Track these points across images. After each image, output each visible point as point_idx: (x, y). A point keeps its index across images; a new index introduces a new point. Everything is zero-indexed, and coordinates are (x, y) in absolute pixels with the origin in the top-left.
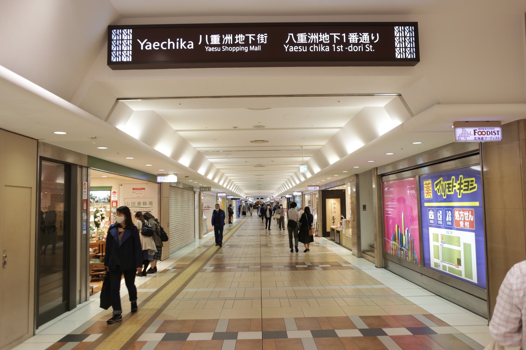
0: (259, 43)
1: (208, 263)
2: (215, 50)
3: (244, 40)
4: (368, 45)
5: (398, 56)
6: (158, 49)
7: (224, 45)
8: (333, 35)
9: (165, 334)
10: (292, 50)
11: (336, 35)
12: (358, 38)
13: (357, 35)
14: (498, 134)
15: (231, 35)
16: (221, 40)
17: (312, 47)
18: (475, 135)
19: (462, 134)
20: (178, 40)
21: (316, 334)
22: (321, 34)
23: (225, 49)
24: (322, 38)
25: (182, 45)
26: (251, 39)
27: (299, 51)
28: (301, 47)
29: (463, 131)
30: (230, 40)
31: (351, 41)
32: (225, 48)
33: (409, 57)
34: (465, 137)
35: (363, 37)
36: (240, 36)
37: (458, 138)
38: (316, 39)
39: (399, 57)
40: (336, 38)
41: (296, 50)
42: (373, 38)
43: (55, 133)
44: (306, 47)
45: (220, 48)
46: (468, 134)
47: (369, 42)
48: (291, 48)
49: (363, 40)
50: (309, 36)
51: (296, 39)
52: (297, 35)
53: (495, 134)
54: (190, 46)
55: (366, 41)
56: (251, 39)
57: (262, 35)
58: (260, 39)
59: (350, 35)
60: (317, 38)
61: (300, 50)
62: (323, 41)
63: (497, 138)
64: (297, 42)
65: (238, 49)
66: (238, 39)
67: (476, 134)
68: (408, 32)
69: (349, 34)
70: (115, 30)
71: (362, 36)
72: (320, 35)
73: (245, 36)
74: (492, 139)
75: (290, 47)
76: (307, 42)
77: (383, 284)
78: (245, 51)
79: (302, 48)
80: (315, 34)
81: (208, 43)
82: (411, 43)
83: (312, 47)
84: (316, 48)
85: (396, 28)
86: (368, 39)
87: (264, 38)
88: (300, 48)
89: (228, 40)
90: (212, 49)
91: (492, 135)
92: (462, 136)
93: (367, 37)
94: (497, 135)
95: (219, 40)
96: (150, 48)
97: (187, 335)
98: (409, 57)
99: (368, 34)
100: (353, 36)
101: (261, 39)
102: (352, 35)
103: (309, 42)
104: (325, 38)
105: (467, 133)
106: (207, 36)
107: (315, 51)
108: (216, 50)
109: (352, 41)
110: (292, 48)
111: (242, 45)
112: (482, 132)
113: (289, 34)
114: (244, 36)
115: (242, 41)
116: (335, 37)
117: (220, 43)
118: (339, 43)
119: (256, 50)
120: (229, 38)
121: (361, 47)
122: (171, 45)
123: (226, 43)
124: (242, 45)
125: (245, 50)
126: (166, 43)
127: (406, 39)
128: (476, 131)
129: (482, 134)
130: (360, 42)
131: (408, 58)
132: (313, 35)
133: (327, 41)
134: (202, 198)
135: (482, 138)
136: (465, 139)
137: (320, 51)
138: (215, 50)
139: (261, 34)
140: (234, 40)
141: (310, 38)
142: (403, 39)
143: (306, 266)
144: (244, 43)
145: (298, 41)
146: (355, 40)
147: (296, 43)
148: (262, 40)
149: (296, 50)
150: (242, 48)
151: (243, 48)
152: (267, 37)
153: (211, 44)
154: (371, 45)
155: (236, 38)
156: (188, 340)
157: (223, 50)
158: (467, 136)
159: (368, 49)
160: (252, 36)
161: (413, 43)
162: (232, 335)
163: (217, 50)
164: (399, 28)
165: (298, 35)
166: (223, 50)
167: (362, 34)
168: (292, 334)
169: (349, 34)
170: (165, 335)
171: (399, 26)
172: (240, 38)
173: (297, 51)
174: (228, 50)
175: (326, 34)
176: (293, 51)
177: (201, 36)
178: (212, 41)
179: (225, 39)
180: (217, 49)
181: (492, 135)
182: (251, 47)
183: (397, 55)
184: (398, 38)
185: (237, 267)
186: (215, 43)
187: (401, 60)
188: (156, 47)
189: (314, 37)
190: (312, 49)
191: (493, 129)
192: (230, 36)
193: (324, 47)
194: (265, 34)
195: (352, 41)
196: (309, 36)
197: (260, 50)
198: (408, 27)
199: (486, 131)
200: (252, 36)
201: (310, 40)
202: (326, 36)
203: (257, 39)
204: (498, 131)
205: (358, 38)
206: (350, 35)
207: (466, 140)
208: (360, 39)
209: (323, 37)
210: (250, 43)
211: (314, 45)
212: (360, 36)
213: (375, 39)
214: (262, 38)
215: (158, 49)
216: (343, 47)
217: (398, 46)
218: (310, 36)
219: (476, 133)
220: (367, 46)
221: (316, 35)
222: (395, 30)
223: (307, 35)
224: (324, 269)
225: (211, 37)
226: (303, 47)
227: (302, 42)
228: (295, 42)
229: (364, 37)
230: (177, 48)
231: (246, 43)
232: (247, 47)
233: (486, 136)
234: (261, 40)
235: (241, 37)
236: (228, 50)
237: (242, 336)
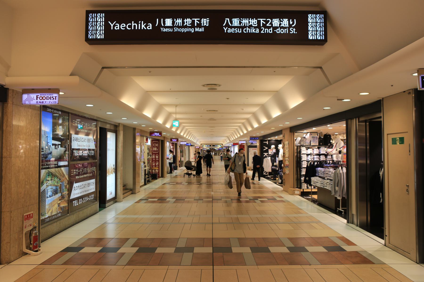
0: (202, 25)
1: (263, 196)
2: (168, 30)
4: (292, 28)
5: (310, 37)
6: (124, 29)
7: (176, 27)
8: (260, 20)
9: (138, 248)
10: (230, 32)
11: (263, 20)
12: (280, 23)
13: (279, 20)
14: (56, 99)
15: (181, 19)
16: (173, 23)
17: (246, 29)
18: (37, 99)
19: (27, 99)
20: (140, 22)
21: (254, 250)
22: (251, 19)
23: (176, 29)
24: (252, 22)
25: (143, 26)
26: (197, 22)
27: (235, 32)
28: (237, 29)
29: (28, 97)
30: (180, 23)
31: (274, 25)
32: (176, 29)
33: (319, 38)
34: (29, 101)
35: (284, 22)
37: (24, 102)
38: (247, 23)
39: (311, 38)
40: (262, 23)
41: (233, 31)
42: (291, 23)
43: (361, 94)
44: (241, 29)
45: (172, 29)
46: (32, 99)
47: (288, 26)
48: (229, 29)
49: (284, 25)
50: (241, 21)
51: (231, 22)
52: (165, 20)
53: (53, 99)
54: (149, 27)
55: (286, 25)
56: (197, 22)
57: (205, 20)
58: (203, 22)
59: (273, 20)
60: (248, 22)
61: (236, 31)
62: (252, 24)
63: (55, 102)
64: (232, 25)
65: (186, 30)
66: (186, 22)
67: (38, 99)
68: (319, 19)
69: (273, 19)
70: (91, 14)
71: (282, 21)
72: (250, 20)
74: (51, 103)
75: (228, 29)
76: (240, 25)
78: (192, 32)
79: (237, 30)
80: (246, 19)
81: (163, 25)
82: (93, 27)
83: (246, 29)
84: (248, 30)
85: (310, 15)
86: (288, 24)
87: (207, 22)
88: (236, 30)
89: (179, 23)
90: (166, 30)
91: (51, 99)
92: (27, 100)
93: (287, 22)
94: (54, 100)
95: (171, 23)
96: (118, 28)
97: (156, 249)
98: (319, 39)
99: (287, 19)
100: (276, 21)
101: (204, 22)
102: (275, 20)
103: (241, 25)
104: (254, 22)
105: (31, 98)
106: (162, 19)
107: (247, 32)
108: (169, 30)
109: (275, 25)
110: (230, 30)
111: (189, 27)
112: (42, 98)
113: (226, 19)
114: (191, 20)
115: (189, 24)
116: (262, 21)
117: (172, 25)
118: (265, 26)
119: (200, 31)
120: (179, 21)
121: (286, 29)
122: (135, 26)
123: (177, 25)
124: (189, 27)
125: (191, 31)
126: (130, 24)
127: (97, 24)
128: (38, 97)
129: (42, 99)
130: (281, 26)
131: (318, 39)
132: (245, 20)
133: (256, 25)
134: (38, 144)
135: (43, 102)
136: (29, 102)
137: (251, 32)
138: (168, 30)
139: (204, 19)
140: (183, 23)
141: (242, 22)
142: (95, 24)
143: (248, 200)
144: (191, 25)
145: (233, 24)
146: (277, 24)
147: (231, 26)
148: (205, 23)
149: (233, 31)
150: (189, 29)
151: (190, 30)
152: (209, 21)
153: (165, 25)
154: (294, 29)
155: (185, 22)
156: (156, 252)
157: (291, 33)
158: (31, 100)
159: (292, 32)
160: (197, 20)
161: (322, 28)
162: (189, 249)
163: (170, 31)
164: (320, 15)
165: (233, 19)
166: (174, 31)
167: (283, 19)
168: (235, 250)
169: (273, 19)
170: (138, 249)
171: (312, 14)
172: (188, 21)
173: (234, 32)
174: (178, 31)
175: (255, 19)
176: (230, 32)
177: (157, 19)
178: (166, 23)
179: (176, 22)
180: (170, 29)
181: (51, 99)
182: (196, 28)
183: (309, 36)
184: (319, 23)
185: (193, 200)
186: (169, 25)
187: (312, 40)
188: (123, 28)
189: (245, 21)
190: (246, 31)
191: (52, 95)
192: (180, 20)
193: (255, 29)
194: (207, 19)
195: (275, 25)
196: (241, 21)
197: (203, 31)
198: (319, 15)
199: (46, 96)
200: (197, 20)
201: (242, 24)
202: (255, 20)
203: (201, 22)
204: (56, 97)
205: (280, 23)
206: (273, 20)
207: (30, 103)
208: (281, 23)
209: (253, 22)
210: (196, 25)
211: (247, 28)
212: (281, 21)
213: (293, 24)
214: (205, 22)
215: (124, 29)
216: (295, 30)
217: (311, 30)
218: (242, 20)
219: (38, 98)
220: (292, 29)
221: (247, 20)
222: (309, 17)
223: (240, 20)
224: (262, 202)
226: (239, 29)
227: (236, 25)
228: (231, 25)
229: (285, 22)
230: (139, 28)
231: (193, 25)
232: (193, 29)
233: (46, 100)
234: (204, 23)
235: (188, 21)
236: (268, 32)
237: (197, 250)
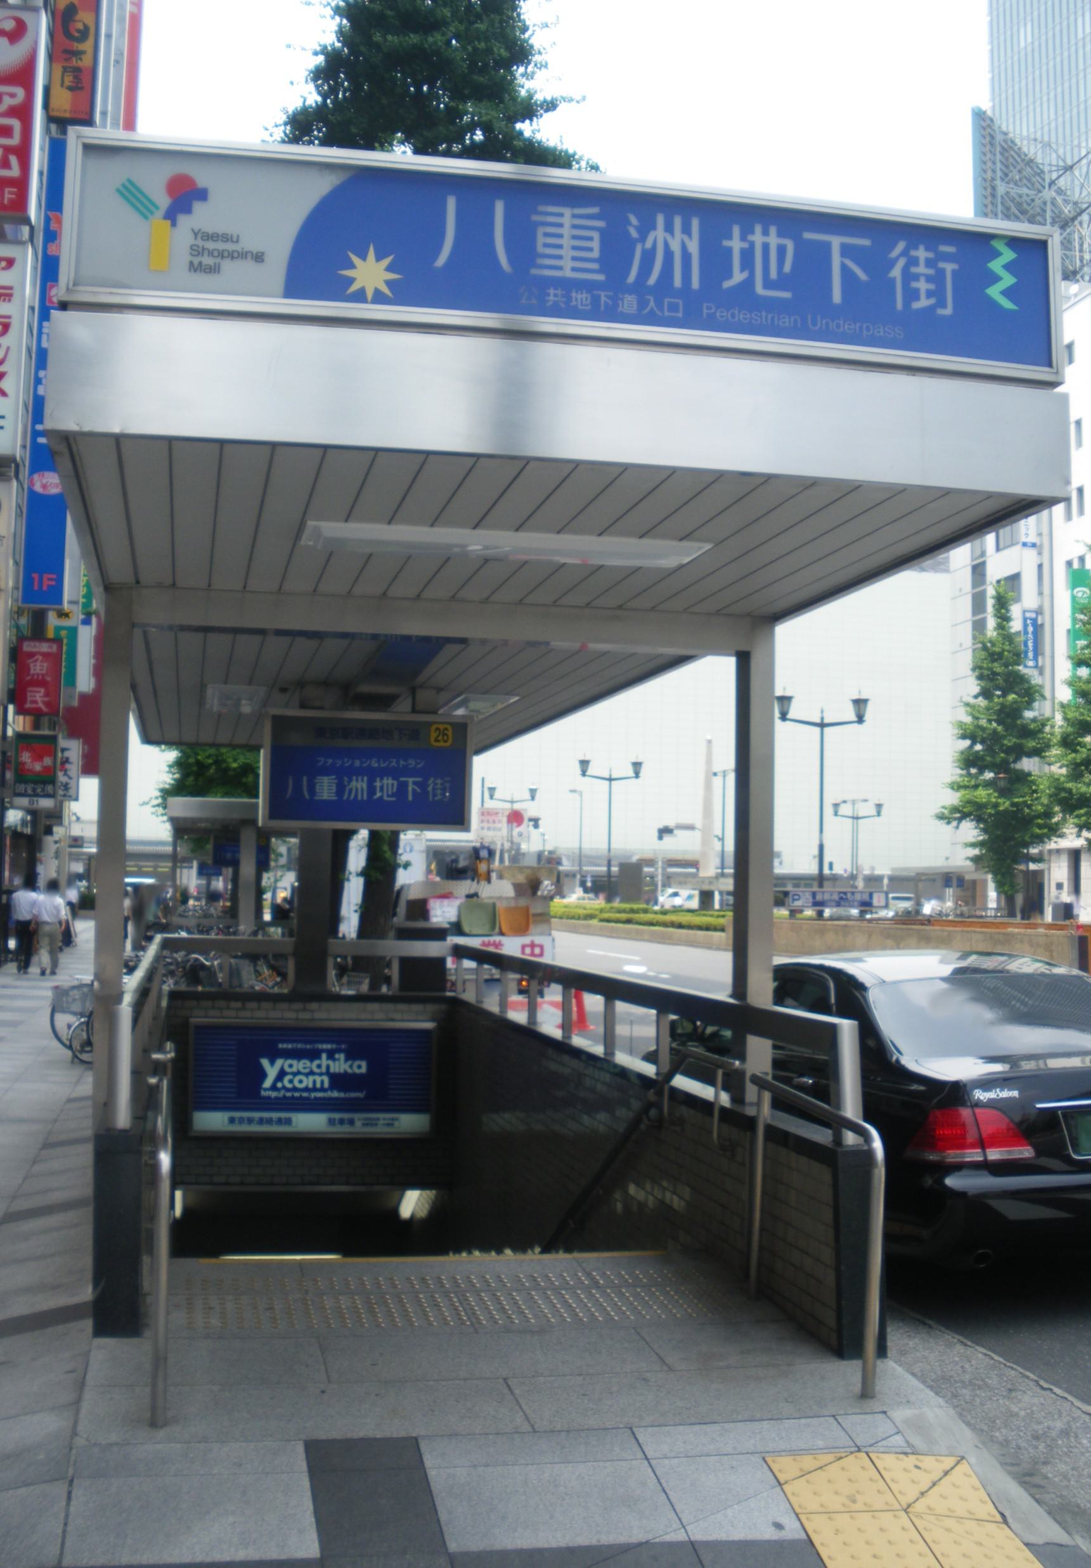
3: (395, 790)
15: (365, 779)
36: (385, 781)
52: (536, 218)
57: (439, 781)
66: (382, 789)
73: (799, 243)
77: (1027, 1545)
87: (938, 278)
114: (395, 783)
115: (390, 793)
144: (394, 799)
152: (954, 266)
179: (649, 244)
225: (316, 781)
